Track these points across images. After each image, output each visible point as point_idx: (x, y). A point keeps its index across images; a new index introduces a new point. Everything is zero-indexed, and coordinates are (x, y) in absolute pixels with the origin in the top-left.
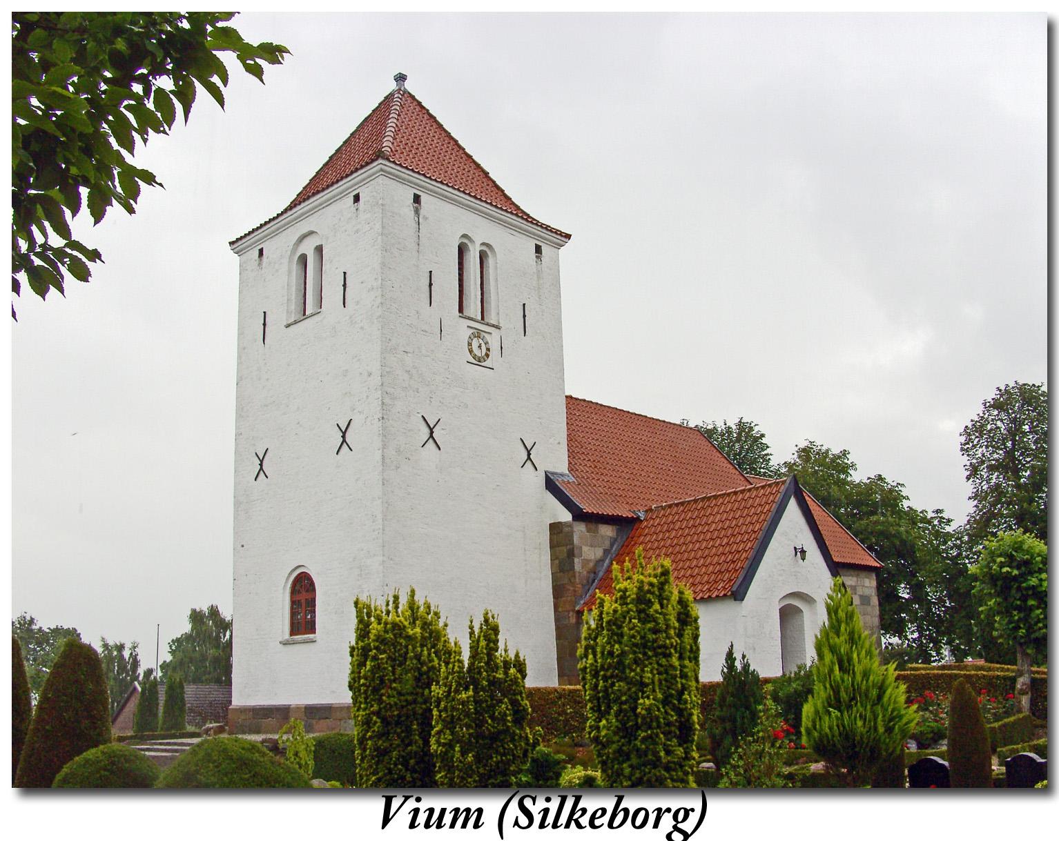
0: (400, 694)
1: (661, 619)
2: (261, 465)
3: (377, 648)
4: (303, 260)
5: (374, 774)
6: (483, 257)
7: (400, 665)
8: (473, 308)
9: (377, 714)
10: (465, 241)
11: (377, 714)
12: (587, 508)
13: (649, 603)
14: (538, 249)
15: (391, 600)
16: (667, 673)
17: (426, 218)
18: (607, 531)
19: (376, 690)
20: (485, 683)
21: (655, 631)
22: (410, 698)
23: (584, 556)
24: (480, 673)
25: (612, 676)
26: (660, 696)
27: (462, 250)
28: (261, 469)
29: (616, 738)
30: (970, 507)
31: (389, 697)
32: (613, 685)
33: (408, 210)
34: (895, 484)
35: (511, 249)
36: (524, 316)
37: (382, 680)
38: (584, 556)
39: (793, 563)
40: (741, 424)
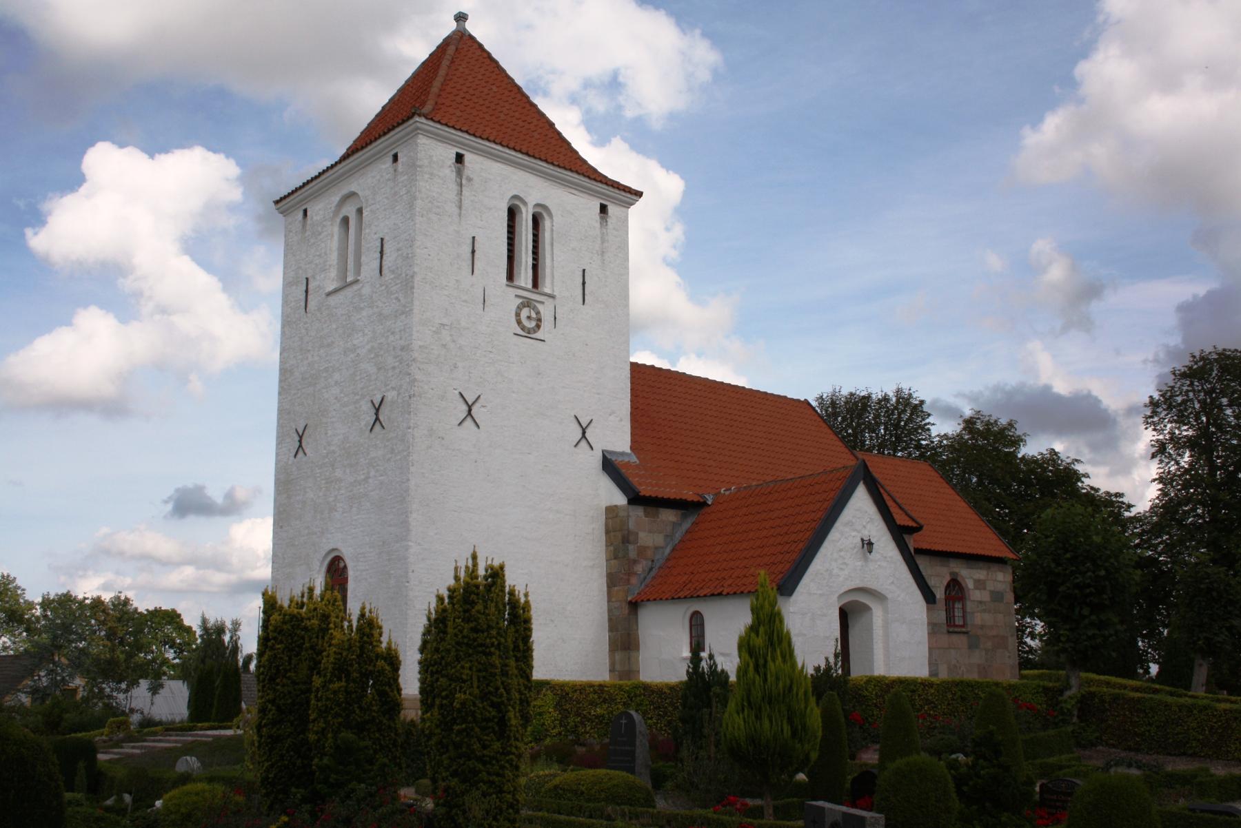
0: (294, 683)
1: (482, 619)
2: (300, 441)
3: (275, 638)
4: (346, 221)
5: (267, 760)
6: (536, 221)
7: (297, 656)
8: (524, 276)
9: (273, 702)
10: (517, 202)
11: (273, 702)
12: (645, 491)
13: (473, 603)
14: (603, 209)
15: (306, 591)
16: (486, 670)
17: (470, 180)
18: (668, 516)
19: (272, 679)
20: (355, 675)
21: (475, 630)
22: (304, 687)
23: (641, 542)
24: (352, 665)
25: (437, 672)
26: (476, 691)
27: (512, 213)
28: (300, 446)
29: (438, 731)
30: (1153, 491)
31: (283, 686)
32: (437, 680)
33: (449, 172)
34: (1069, 461)
35: (569, 207)
36: (584, 283)
37: (277, 667)
38: (641, 542)
39: (857, 553)
40: (899, 392)
